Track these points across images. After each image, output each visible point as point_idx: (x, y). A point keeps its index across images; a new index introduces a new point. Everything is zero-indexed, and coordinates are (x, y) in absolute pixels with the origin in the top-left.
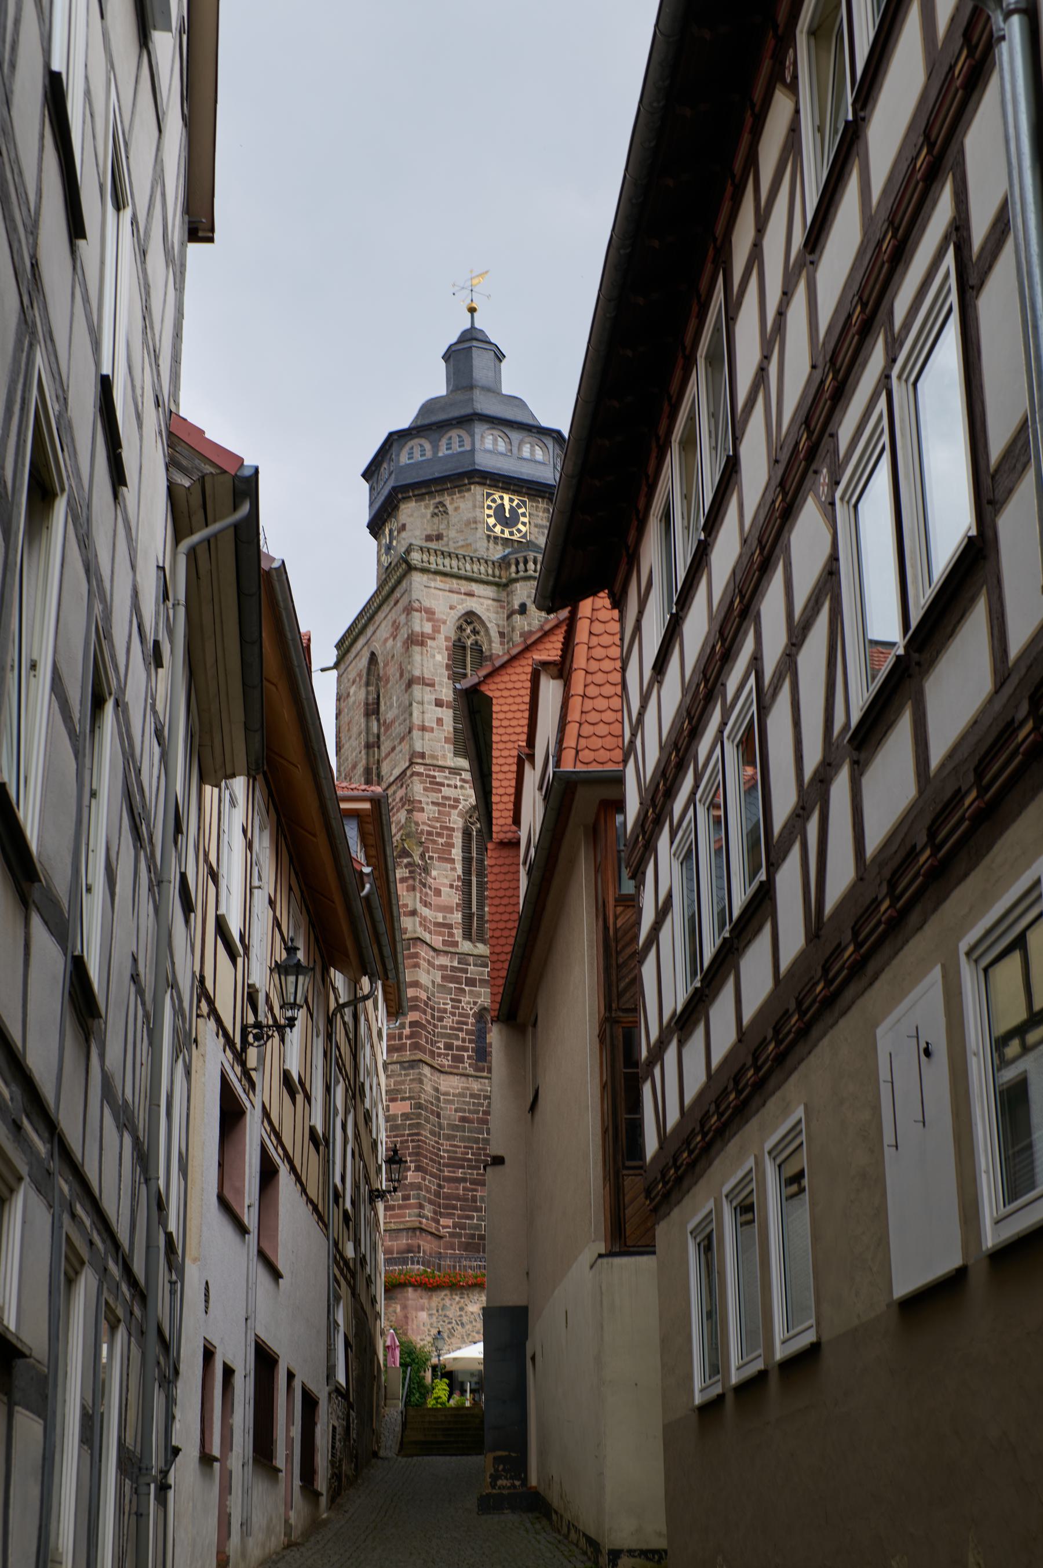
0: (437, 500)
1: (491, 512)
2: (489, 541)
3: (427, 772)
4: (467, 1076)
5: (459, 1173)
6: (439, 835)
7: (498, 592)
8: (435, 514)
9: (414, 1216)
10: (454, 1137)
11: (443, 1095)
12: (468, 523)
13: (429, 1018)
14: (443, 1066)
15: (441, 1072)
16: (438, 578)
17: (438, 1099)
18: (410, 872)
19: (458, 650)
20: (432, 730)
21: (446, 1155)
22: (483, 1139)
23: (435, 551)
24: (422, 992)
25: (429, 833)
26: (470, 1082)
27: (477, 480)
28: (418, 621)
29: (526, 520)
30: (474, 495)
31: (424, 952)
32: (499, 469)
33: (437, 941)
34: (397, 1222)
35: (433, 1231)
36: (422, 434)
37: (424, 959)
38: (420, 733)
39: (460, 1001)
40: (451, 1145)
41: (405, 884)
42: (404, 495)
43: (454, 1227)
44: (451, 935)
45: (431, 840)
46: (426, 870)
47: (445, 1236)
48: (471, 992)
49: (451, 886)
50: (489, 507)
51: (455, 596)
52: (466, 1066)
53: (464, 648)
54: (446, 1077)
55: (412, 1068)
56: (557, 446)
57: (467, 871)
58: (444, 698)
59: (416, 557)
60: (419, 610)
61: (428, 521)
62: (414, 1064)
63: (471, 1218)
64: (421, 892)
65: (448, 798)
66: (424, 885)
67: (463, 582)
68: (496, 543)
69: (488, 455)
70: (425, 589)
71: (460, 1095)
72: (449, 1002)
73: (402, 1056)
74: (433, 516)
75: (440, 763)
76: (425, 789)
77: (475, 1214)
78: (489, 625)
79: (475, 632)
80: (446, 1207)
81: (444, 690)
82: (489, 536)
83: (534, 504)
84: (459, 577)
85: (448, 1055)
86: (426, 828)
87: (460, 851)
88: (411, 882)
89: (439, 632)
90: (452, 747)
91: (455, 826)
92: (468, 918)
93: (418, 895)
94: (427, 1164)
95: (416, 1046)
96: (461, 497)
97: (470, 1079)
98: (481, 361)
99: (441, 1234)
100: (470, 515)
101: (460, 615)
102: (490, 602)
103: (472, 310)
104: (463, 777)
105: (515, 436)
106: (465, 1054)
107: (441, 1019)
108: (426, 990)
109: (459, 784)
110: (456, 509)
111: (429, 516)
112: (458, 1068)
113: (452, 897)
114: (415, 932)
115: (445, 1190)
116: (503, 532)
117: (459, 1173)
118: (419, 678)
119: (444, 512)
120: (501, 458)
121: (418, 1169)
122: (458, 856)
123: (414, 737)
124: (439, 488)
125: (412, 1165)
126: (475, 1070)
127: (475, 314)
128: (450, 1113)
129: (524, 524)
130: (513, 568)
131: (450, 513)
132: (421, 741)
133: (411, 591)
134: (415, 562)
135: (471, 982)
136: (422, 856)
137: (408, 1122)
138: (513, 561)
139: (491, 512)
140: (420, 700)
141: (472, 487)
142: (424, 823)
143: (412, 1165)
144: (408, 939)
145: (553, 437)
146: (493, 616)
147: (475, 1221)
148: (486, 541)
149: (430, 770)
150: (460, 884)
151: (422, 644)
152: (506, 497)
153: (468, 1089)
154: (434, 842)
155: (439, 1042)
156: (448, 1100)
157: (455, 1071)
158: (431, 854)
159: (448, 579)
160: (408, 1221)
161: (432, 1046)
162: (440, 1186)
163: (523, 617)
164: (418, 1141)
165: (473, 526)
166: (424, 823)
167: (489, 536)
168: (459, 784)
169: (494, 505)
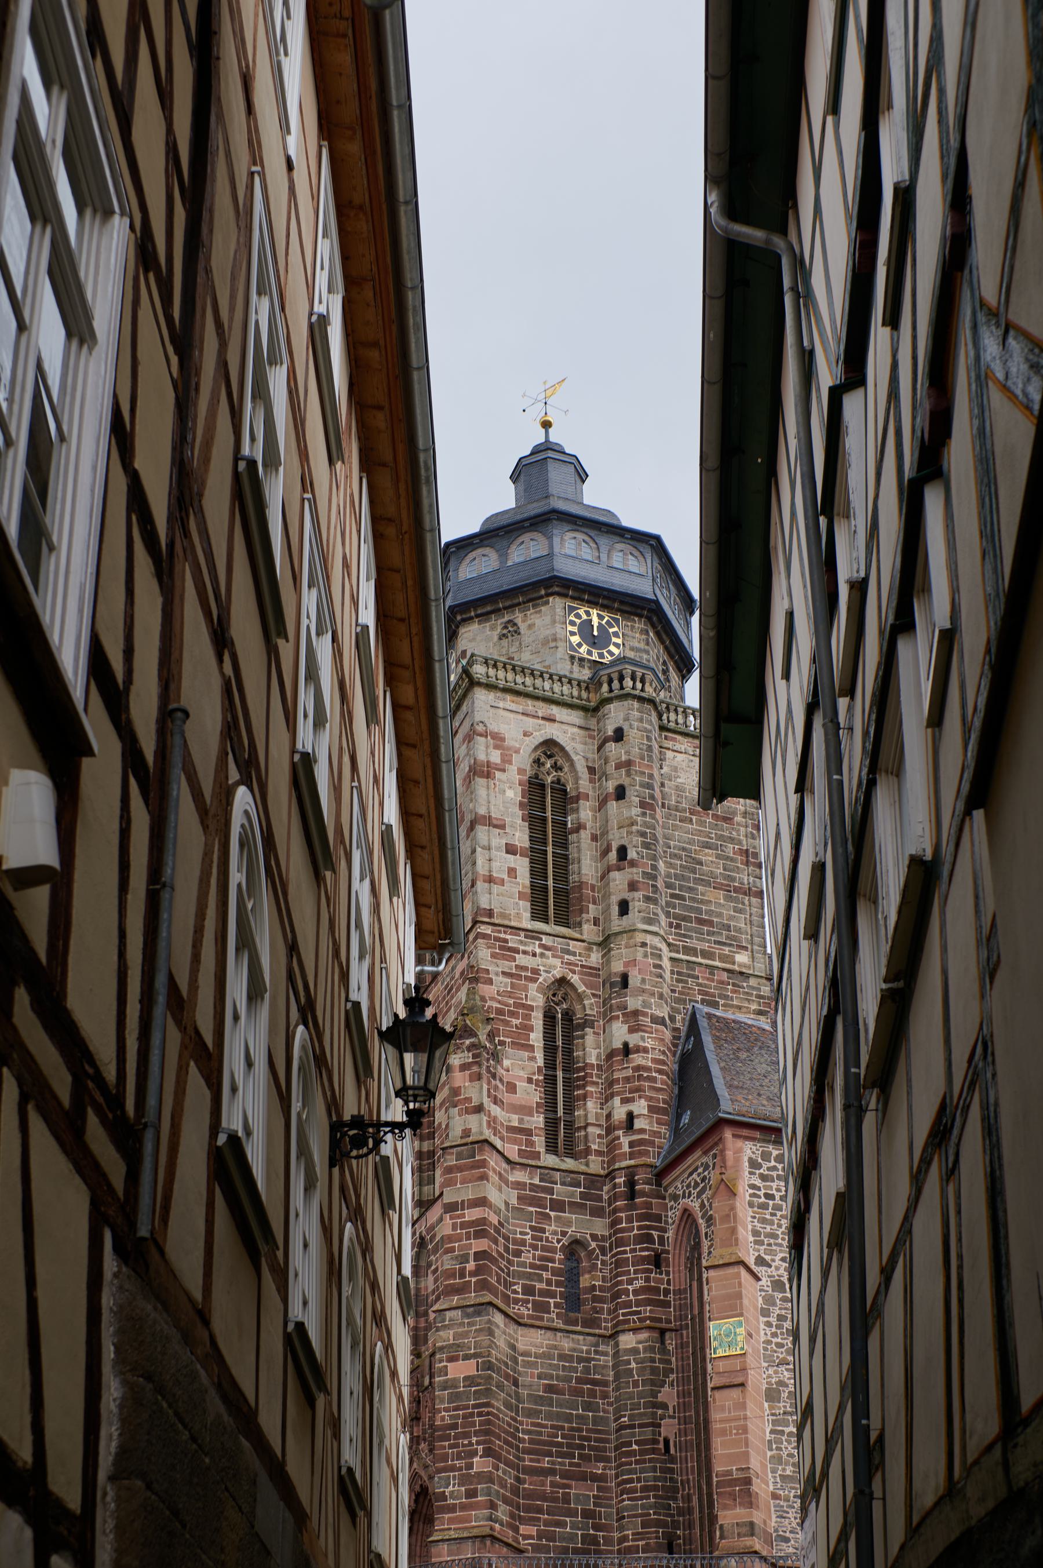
0: (506, 619)
1: (575, 629)
2: (573, 664)
3: (496, 934)
4: (555, 1330)
5: (546, 1463)
6: (512, 1014)
7: (586, 718)
8: (504, 635)
9: (485, 1323)
10: (536, 1413)
11: (522, 1355)
12: (545, 642)
13: (501, 1249)
14: (522, 1316)
15: (519, 1324)
16: (508, 697)
17: (515, 1360)
18: (474, 1056)
19: (535, 788)
20: (502, 882)
21: (526, 1437)
22: (577, 1416)
23: (505, 664)
24: (491, 1213)
25: (500, 1012)
26: (558, 1339)
27: (557, 589)
28: (482, 748)
29: (619, 641)
30: (554, 608)
31: (493, 1161)
32: (585, 578)
33: (512, 1151)
34: (459, 1529)
35: (510, 1541)
36: (486, 542)
37: (494, 1170)
38: (487, 885)
39: (543, 1231)
40: (533, 1424)
41: (467, 1072)
42: (464, 616)
43: (539, 1538)
44: (530, 1143)
45: (502, 1020)
46: (495, 1056)
47: (526, 1551)
48: (557, 1218)
49: (530, 1081)
50: (572, 623)
51: (531, 720)
52: (553, 1317)
53: (542, 786)
54: (526, 1330)
55: (479, 1314)
56: (655, 557)
57: (550, 1064)
58: (517, 843)
59: (479, 670)
60: (484, 735)
61: (495, 644)
62: (480, 1308)
63: (562, 1524)
64: (489, 1083)
65: (524, 968)
66: (494, 1076)
67: (540, 704)
68: (582, 666)
69: (570, 561)
70: (492, 710)
71: (544, 1356)
72: (528, 1230)
73: (465, 1299)
74: (500, 639)
75: (513, 924)
76: (494, 956)
77: (568, 1519)
78: (575, 758)
79: (556, 767)
80: (528, 1509)
81: (517, 834)
82: (572, 657)
83: (629, 624)
84: (537, 698)
85: (527, 1301)
86: (495, 1005)
87: (541, 1035)
88: (475, 1069)
89: (510, 762)
90: (529, 904)
92: (552, 1125)
93: (485, 1087)
94: (501, 1447)
95: (483, 1285)
96: (536, 612)
97: (559, 1334)
98: (558, 477)
99: (521, 1547)
100: (548, 632)
101: (537, 743)
102: (576, 730)
103: (546, 425)
104: (543, 942)
105: (604, 541)
106: (552, 1301)
107: (518, 1254)
108: (497, 1212)
109: (538, 951)
110: (531, 627)
111: (496, 638)
112: (542, 1319)
113: (531, 1095)
114: (481, 1133)
115: (526, 1486)
116: (590, 653)
117: (546, 1463)
118: (485, 817)
119: (516, 632)
120: (588, 566)
121: (488, 1453)
122: (538, 1042)
123: (479, 890)
124: (508, 603)
125: (480, 1448)
126: (566, 1323)
127: (551, 430)
128: (530, 1379)
129: (617, 645)
130: (605, 687)
131: (522, 631)
132: (488, 896)
133: (473, 712)
134: (479, 676)
135: (558, 1206)
136: (491, 1036)
137: (473, 1389)
138: (605, 678)
139: (575, 629)
140: (486, 843)
141: (551, 599)
142: (492, 999)
143: (480, 1448)
144: (472, 1143)
145: (651, 545)
146: (580, 747)
147: (568, 1529)
148: (569, 663)
150: (541, 1078)
151: (488, 776)
152: (594, 613)
153: (555, 1347)
154: (507, 1023)
155: (515, 1284)
156: (528, 1362)
157: (538, 1323)
158: (502, 1038)
159: (520, 699)
160: (474, 1527)
161: (505, 1287)
162: (518, 1479)
163: (619, 744)
164: (488, 1413)
165: (553, 644)
166: (492, 999)
167: (572, 657)
168: (538, 951)
169: (578, 621)
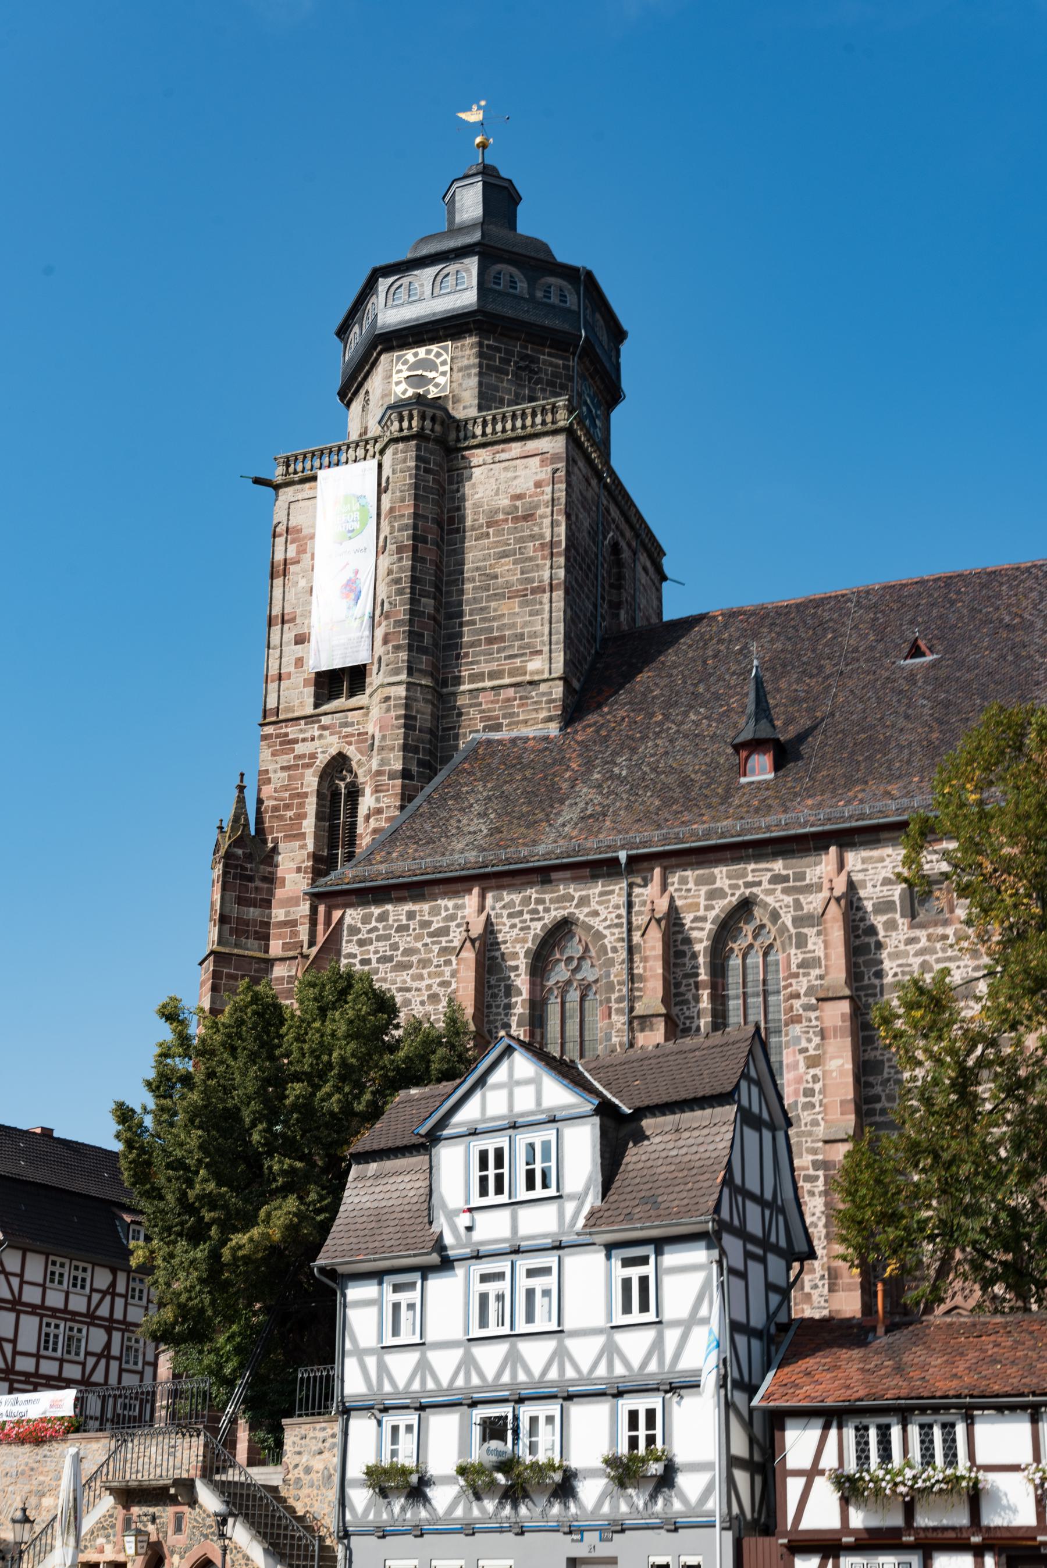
6: (287, 807)
45: (277, 817)
49: (299, 870)
91: (309, 790)
149: (281, 728)
154: (281, 818)
168: (317, 733)
